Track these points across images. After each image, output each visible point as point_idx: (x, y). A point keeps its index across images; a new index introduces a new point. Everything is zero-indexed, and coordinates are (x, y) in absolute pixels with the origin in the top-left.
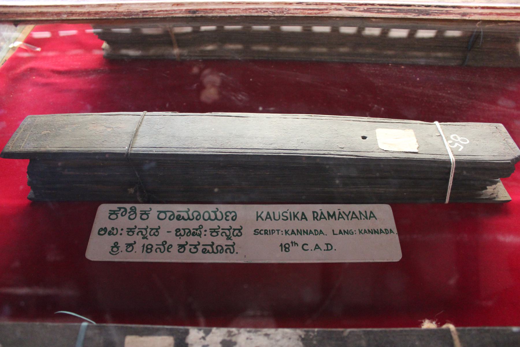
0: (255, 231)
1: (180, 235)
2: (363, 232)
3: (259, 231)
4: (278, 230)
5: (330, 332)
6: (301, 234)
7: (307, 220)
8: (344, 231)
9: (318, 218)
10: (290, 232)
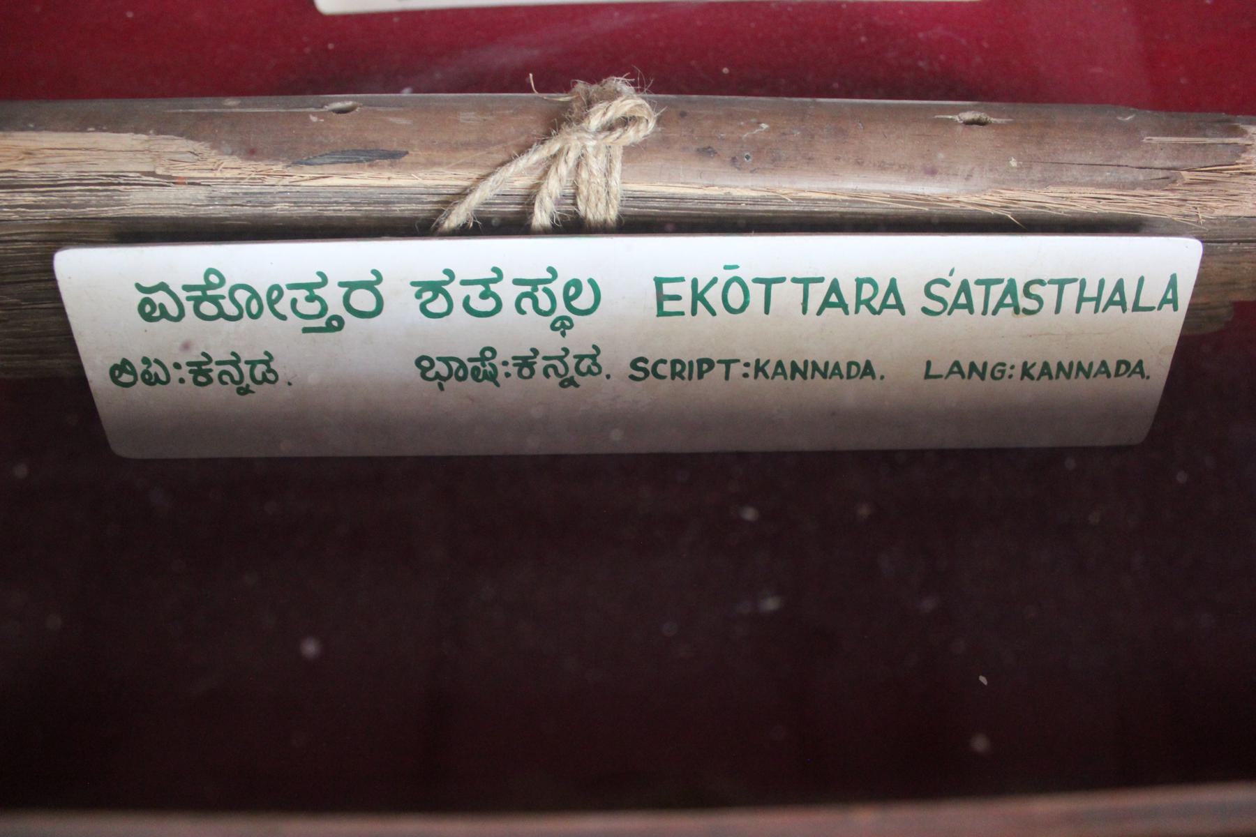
0: (634, 365)
1: (438, 376)
2: (770, 370)
3: (649, 367)
4: (728, 363)
5: (852, 104)
6: (805, 377)
7: (903, 313)
8: (973, 366)
9: (876, 304)
10: (770, 370)
